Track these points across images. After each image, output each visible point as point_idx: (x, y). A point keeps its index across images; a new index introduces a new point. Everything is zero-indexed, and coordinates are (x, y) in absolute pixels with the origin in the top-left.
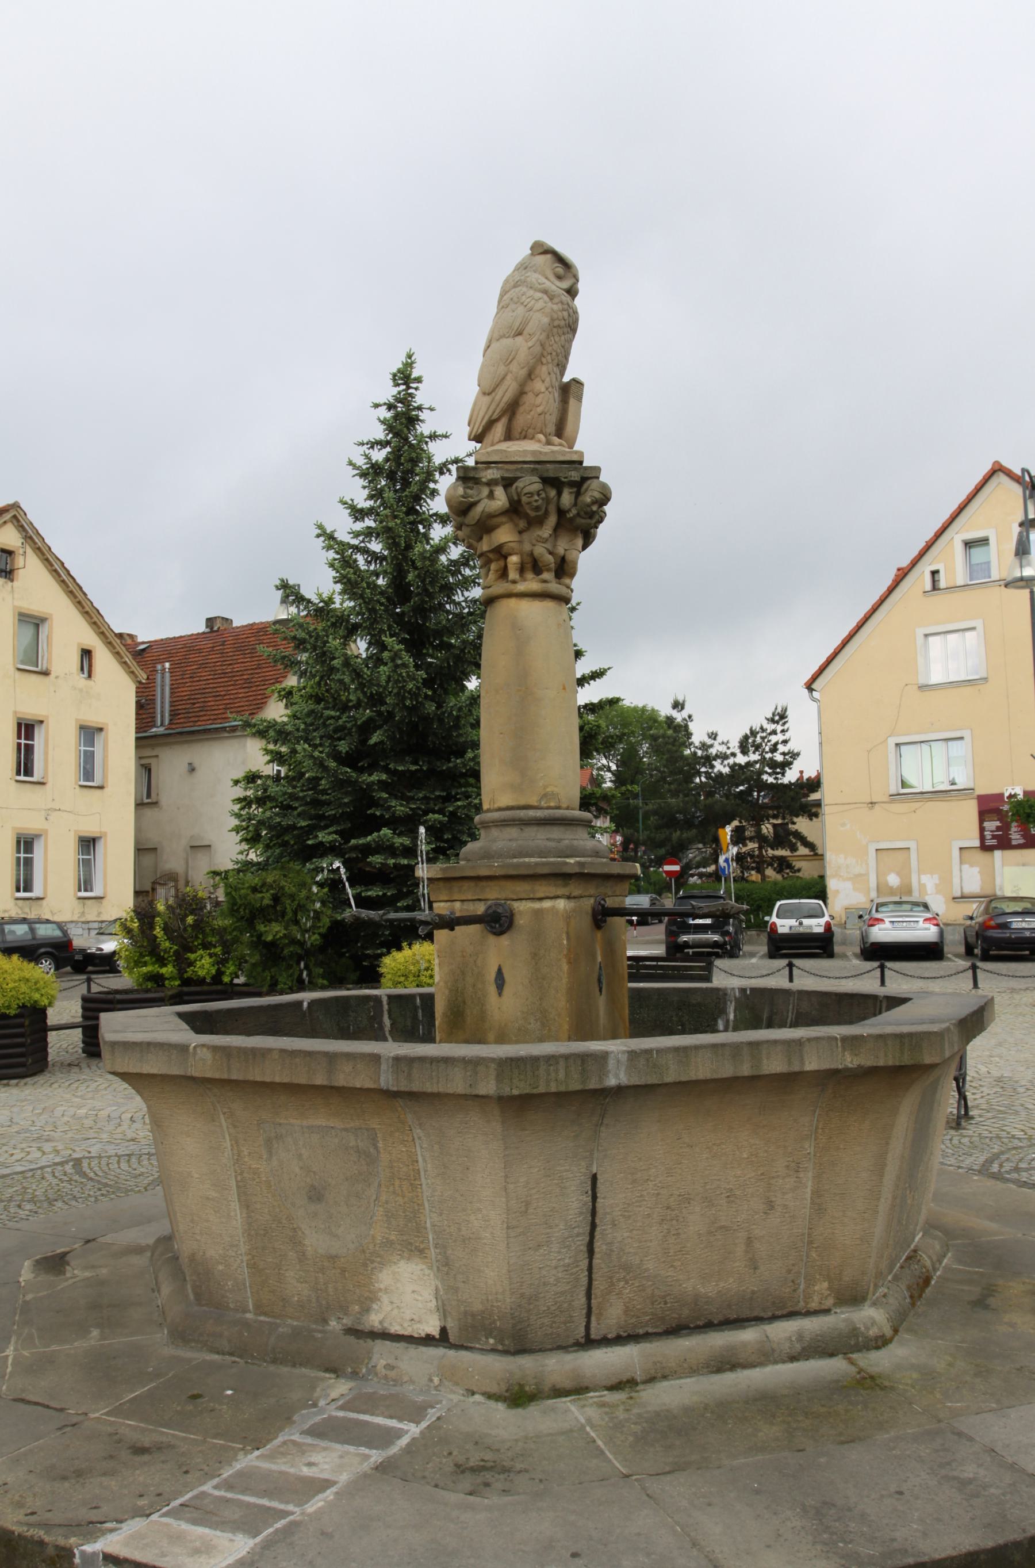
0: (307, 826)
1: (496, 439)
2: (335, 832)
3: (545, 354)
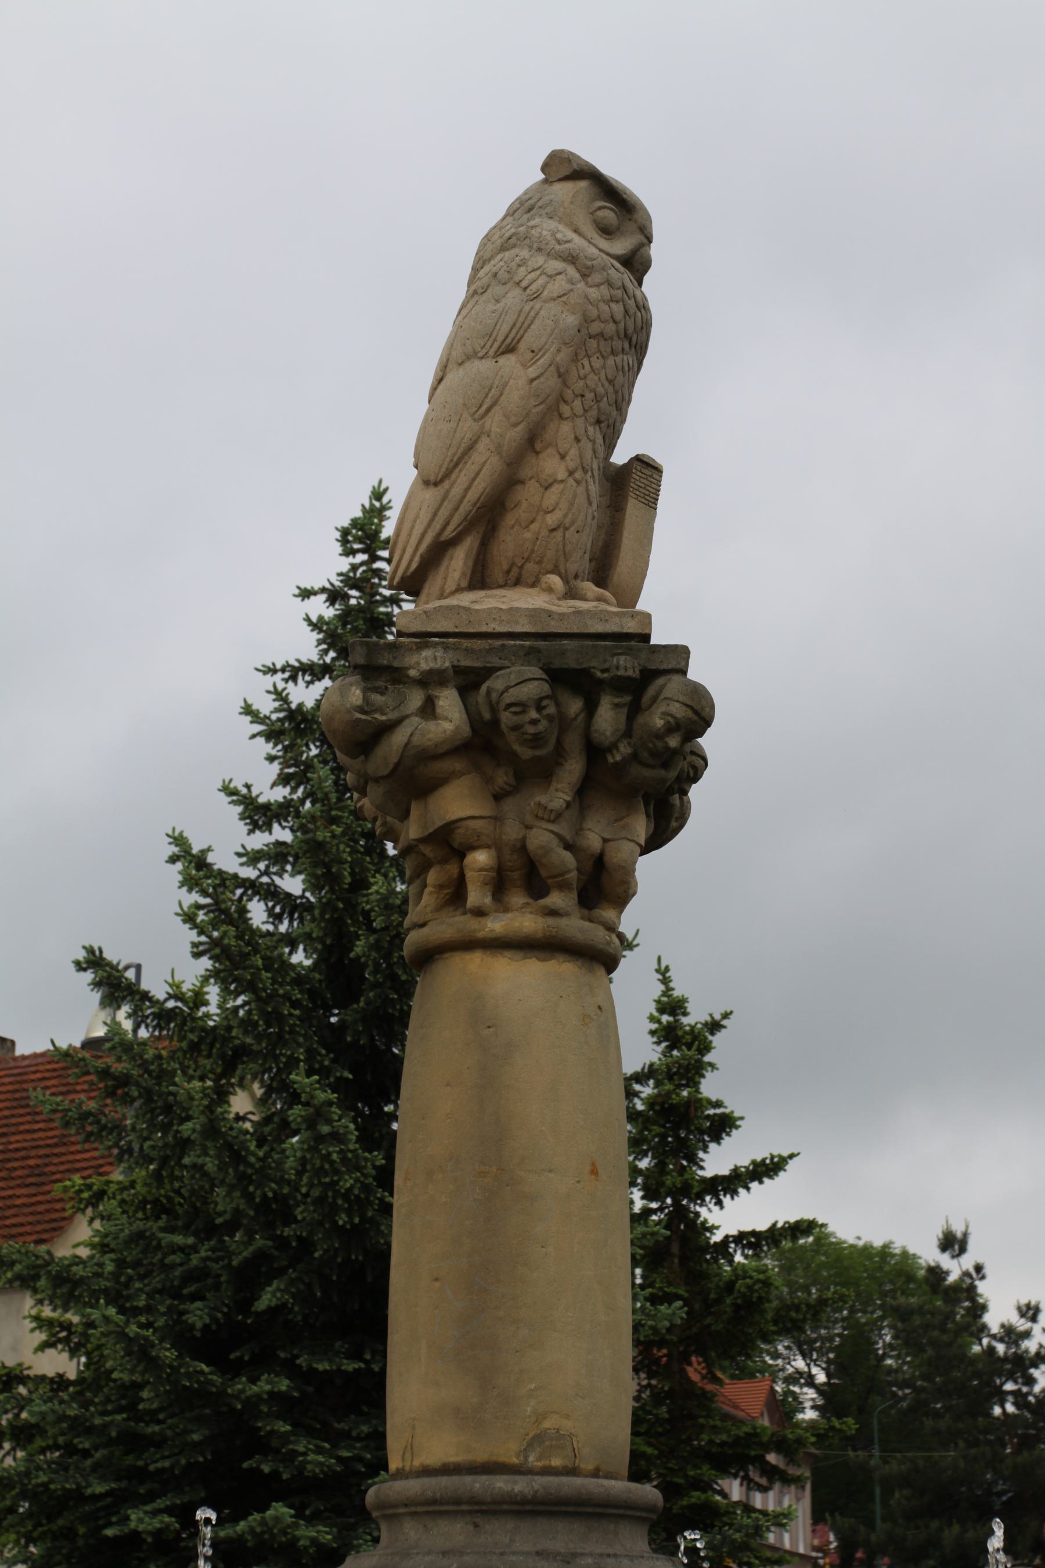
0: (108, 1494)
1: (451, 586)
2: (168, 1511)
3: (568, 394)
